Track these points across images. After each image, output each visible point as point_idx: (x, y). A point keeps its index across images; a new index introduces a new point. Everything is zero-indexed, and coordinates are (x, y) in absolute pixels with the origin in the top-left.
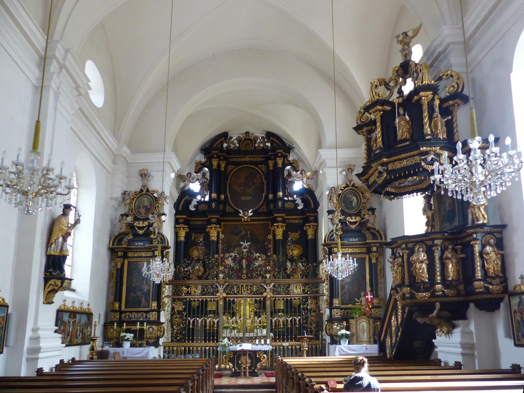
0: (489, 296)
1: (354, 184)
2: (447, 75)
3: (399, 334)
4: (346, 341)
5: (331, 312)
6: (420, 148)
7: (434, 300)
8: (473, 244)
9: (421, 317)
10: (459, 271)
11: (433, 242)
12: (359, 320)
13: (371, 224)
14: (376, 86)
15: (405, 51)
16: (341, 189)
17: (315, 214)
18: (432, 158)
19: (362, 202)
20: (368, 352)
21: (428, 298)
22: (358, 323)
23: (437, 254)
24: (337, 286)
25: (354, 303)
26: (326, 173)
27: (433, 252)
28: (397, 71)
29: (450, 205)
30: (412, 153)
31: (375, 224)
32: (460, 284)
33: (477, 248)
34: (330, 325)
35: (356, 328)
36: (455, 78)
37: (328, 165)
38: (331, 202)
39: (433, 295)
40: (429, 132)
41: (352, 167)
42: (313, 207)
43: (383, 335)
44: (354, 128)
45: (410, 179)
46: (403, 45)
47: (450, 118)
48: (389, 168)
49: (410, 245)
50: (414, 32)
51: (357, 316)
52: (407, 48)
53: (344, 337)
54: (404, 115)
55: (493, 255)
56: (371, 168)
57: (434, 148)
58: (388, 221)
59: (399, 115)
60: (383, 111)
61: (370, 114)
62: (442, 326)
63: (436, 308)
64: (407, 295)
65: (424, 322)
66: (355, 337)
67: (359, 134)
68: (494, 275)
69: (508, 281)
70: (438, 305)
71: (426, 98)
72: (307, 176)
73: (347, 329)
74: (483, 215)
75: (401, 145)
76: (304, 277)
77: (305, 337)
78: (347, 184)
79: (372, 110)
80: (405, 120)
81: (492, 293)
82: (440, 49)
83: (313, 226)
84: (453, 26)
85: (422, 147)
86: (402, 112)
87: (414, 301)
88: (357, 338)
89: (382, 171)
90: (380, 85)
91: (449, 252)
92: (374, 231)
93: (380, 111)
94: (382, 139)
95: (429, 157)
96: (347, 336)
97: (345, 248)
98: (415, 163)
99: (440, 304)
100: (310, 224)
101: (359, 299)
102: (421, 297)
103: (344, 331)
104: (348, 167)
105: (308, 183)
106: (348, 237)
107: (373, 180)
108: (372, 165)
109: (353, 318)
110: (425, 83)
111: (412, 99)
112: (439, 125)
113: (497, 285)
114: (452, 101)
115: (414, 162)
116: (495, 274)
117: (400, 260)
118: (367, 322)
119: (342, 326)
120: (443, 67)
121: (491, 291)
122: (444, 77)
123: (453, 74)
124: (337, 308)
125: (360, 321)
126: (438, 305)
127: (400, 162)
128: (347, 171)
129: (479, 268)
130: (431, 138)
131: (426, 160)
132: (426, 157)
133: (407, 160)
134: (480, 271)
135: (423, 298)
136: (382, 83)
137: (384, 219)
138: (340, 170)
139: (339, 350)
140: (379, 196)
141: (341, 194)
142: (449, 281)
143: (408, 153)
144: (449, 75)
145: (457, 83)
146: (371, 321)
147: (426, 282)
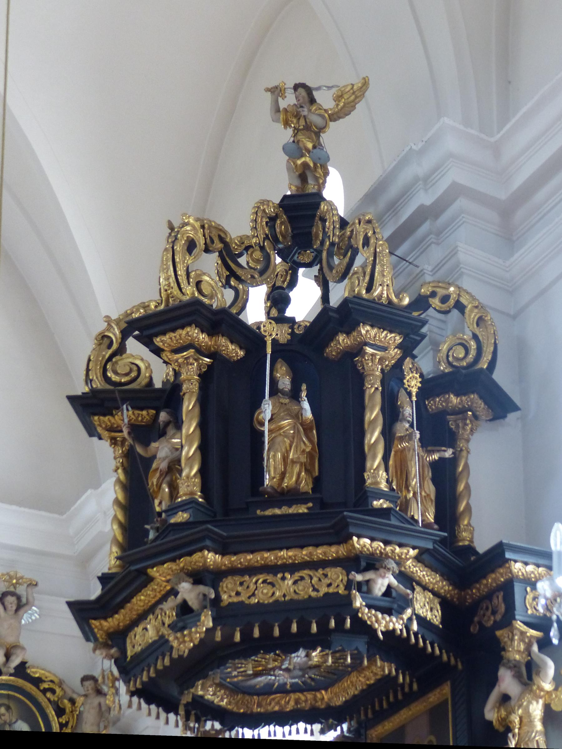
1: (23, 665)
6: (351, 538)
14: (191, 246)
15: (302, 156)
18: (389, 587)
28: (272, 220)
30: (319, 553)
36: (472, 316)
40: (383, 486)
41: (21, 590)
44: (72, 399)
45: (299, 657)
46: (297, 131)
47: (448, 453)
48: (225, 597)
50: (338, 98)
52: (310, 145)
54: (295, 395)
56: (144, 585)
57: (398, 550)
59: (274, 391)
60: (214, 355)
61: (157, 351)
67: (91, 431)
71: (379, 354)
75: (277, 511)
79: (166, 338)
80: (297, 416)
85: (359, 537)
86: (285, 383)
89: (194, 603)
90: (207, 250)
94: (202, 472)
98: (326, 594)
107: (151, 635)
108: (153, 572)
110: (380, 296)
111: (327, 345)
112: (414, 469)
114: (457, 395)
115: (324, 590)
120: (428, 268)
122: (435, 302)
123: (463, 300)
127: (270, 578)
130: (388, 510)
131: (369, 591)
132: (369, 575)
133: (297, 576)
136: (212, 241)
140: (163, 715)
143: (302, 547)
144: (452, 302)
145: (475, 337)
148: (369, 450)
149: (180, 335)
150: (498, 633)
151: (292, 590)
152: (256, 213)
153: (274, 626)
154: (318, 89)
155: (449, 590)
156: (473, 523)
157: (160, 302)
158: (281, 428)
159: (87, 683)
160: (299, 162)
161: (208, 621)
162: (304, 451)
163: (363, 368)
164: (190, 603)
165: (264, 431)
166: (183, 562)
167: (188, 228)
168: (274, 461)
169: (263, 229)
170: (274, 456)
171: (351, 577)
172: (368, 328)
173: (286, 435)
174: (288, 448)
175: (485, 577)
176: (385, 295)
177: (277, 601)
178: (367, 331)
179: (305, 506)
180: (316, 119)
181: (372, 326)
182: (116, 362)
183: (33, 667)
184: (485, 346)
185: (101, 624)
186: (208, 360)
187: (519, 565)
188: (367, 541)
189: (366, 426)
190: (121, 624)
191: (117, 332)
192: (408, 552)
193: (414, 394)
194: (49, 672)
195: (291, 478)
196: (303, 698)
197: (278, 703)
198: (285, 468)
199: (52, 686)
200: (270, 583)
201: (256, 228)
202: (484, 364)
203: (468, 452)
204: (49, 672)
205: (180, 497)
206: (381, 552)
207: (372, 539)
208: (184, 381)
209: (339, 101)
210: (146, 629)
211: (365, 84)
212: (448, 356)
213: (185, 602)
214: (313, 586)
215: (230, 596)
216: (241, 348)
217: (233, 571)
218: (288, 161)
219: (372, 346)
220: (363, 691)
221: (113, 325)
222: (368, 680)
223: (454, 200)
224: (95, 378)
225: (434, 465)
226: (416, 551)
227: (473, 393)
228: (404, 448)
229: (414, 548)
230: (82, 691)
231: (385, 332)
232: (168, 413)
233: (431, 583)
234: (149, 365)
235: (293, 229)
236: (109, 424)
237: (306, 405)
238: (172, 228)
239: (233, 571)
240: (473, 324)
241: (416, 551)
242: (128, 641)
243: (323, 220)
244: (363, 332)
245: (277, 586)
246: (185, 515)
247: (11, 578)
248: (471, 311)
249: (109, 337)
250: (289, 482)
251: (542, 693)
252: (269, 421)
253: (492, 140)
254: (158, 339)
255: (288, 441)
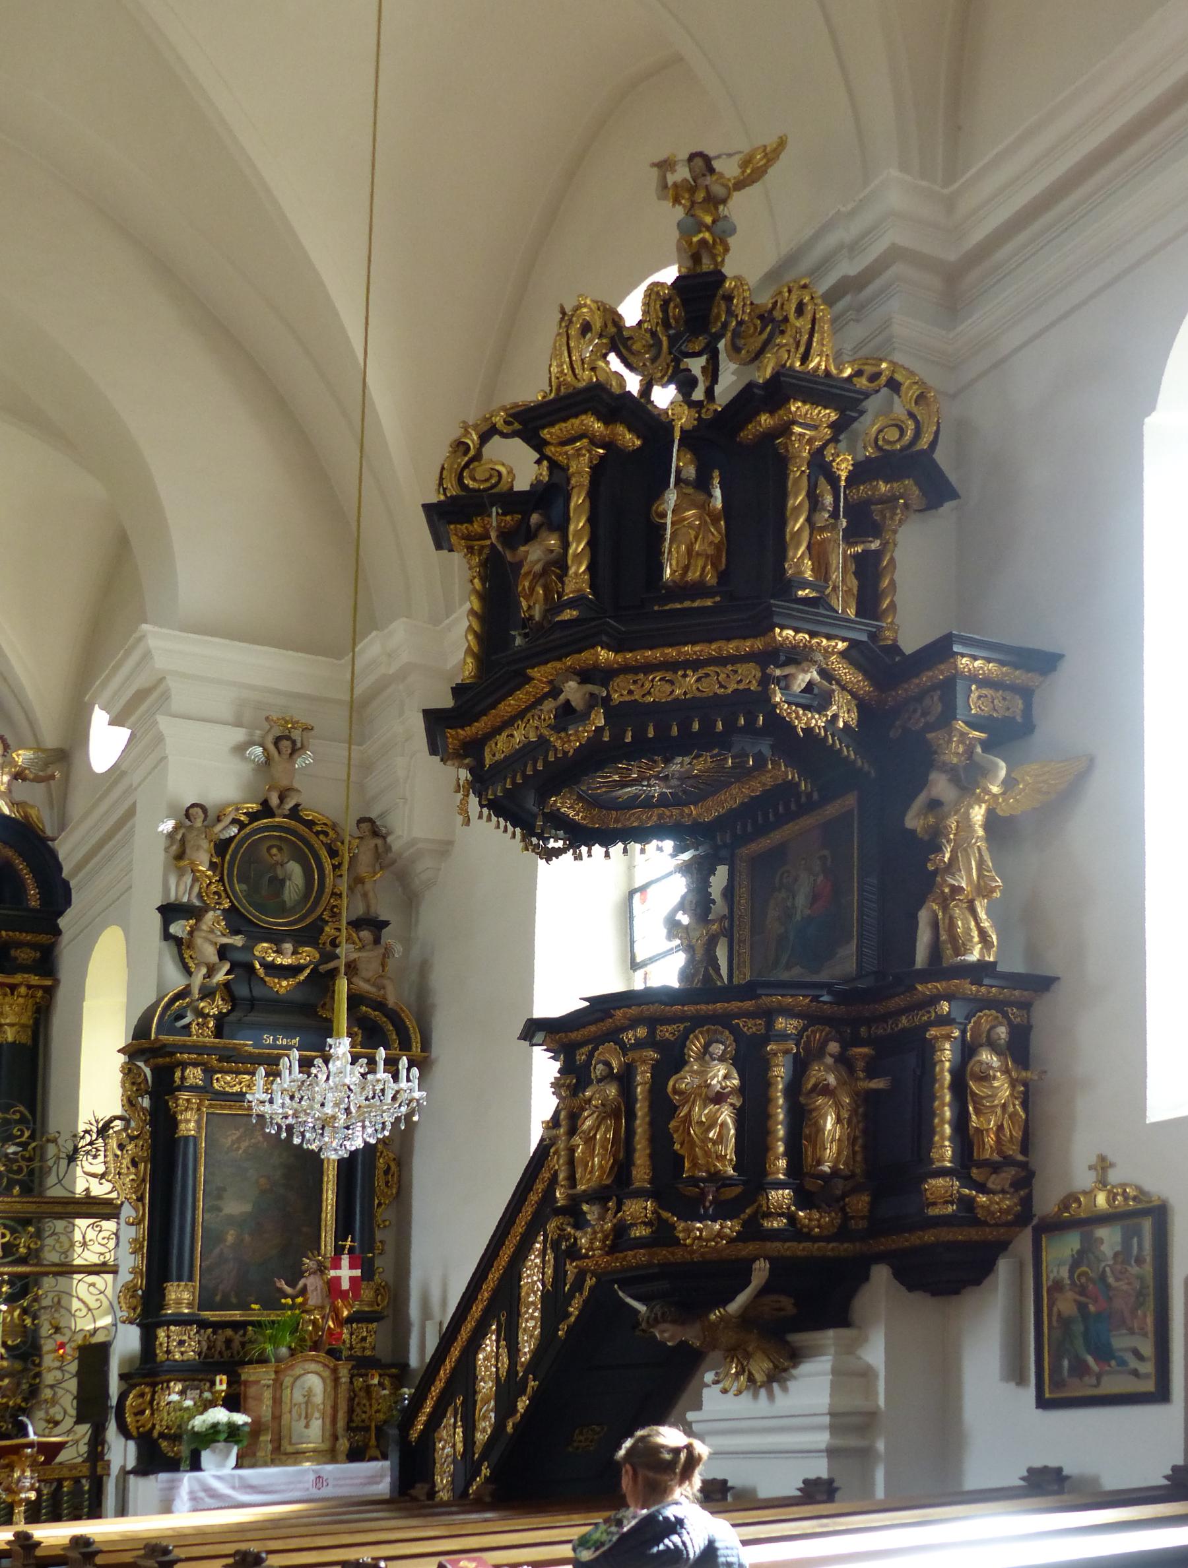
0: (973, 1234)
2: (874, 377)
3: (522, 1404)
4: (227, 1455)
5: (148, 1339)
6: (773, 630)
7: (751, 1248)
8: (936, 1038)
9: (674, 1322)
10: (855, 1139)
11: (770, 1025)
12: (291, 1367)
13: (367, 981)
14: (586, 328)
15: (700, 232)
16: (235, 821)
17: (43, 938)
19: (328, 890)
20: (327, 1492)
21: (731, 1241)
22: (288, 1381)
23: (780, 1072)
24: (188, 1229)
25: (272, 1302)
26: (168, 740)
27: (765, 1064)
29: (815, 898)
30: (731, 648)
31: (386, 982)
32: (855, 1190)
33: (947, 1055)
34: (142, 1395)
35: (277, 1401)
37: (178, 702)
38: (181, 873)
39: (752, 1231)
40: (808, 575)
41: (296, 735)
42: (34, 903)
43: (422, 1418)
47: (875, 545)
49: (666, 1032)
50: (745, 164)
51: (284, 1351)
53: (223, 1436)
55: (1002, 1088)
57: (825, 642)
58: (441, 980)
60: (609, 445)
62: (748, 1356)
63: (749, 1282)
64: (640, 1232)
65: (681, 1342)
66: (266, 1438)
68: (996, 1157)
69: (1037, 1183)
70: (761, 1271)
72: (13, 763)
73: (233, 1403)
74: (983, 934)
76: (17, 1190)
77: (31, 1445)
78: (265, 803)
79: (555, 430)
81: (985, 1223)
82: (848, 268)
83: (29, 987)
84: (924, 183)
85: (782, 628)
86: (690, 472)
87: (663, 1254)
88: (280, 1439)
91: (828, 1069)
92: (374, 1014)
93: (594, 442)
95: (801, 677)
96: (233, 1433)
97: (238, 1073)
98: (736, 690)
99: (771, 1270)
100: (18, 978)
101: (292, 1285)
102: (700, 1238)
103: (220, 1415)
104: (277, 732)
105: (18, 797)
106: (252, 1026)
108: (535, 673)
109: (262, 1360)
113: (1003, 1191)
114: (886, 483)
115: (732, 687)
116: (1000, 1152)
117: (612, 1091)
118: (327, 1373)
119: (207, 1395)
121: (980, 1214)
123: (898, 377)
124: (181, 1321)
125: (298, 1371)
126: (761, 1271)
128: (271, 748)
129: (947, 1129)
132: (787, 671)
133: (701, 673)
134: (951, 1139)
135: (708, 1240)
137: (424, 969)
138: (239, 735)
139: (191, 1492)
141: (232, 839)
142: (822, 1176)
143: (710, 641)
144: (883, 379)
146: (344, 1373)
147: (730, 1178)
148: (792, 538)
149: (572, 425)
150: (930, 736)
151: (694, 688)
152: (650, 295)
153: (671, 725)
154: (719, 157)
155: (870, 692)
156: (897, 621)
157: (548, 392)
158: (684, 519)
159: (363, 825)
160: (695, 239)
161: (600, 719)
162: (711, 543)
163: (787, 451)
164: (573, 704)
165: (666, 524)
166: (569, 661)
167: (585, 310)
168: (678, 553)
169: (657, 313)
170: (678, 547)
171: (768, 671)
172: (799, 404)
173: (690, 526)
174: (693, 540)
175: (917, 675)
176: (823, 367)
177: (677, 700)
178: (798, 408)
179: (712, 600)
180: (718, 190)
181: (804, 402)
182: (474, 469)
183: (306, 810)
184: (926, 425)
185: (457, 733)
186: (601, 451)
187: (965, 660)
188: (791, 633)
189: (788, 513)
190: (480, 733)
191: (475, 437)
192: (837, 644)
193: (843, 478)
194: (323, 816)
195: (694, 573)
196: (668, 813)
197: (638, 818)
198: (689, 561)
199: (325, 828)
200: (668, 681)
201: (648, 312)
202: (924, 444)
203: (895, 545)
204: (323, 816)
205: (567, 594)
206: (805, 644)
207: (797, 631)
208: (573, 474)
209: (747, 167)
210: (512, 736)
211: (782, 144)
212: (876, 440)
213: (568, 702)
214: (719, 683)
215: (622, 695)
216: (638, 438)
217: (626, 669)
218: (678, 241)
219: (801, 425)
220: (743, 804)
221: (470, 430)
222: (753, 791)
223: (887, 267)
224: (449, 486)
225: (856, 557)
226: (846, 644)
227: (908, 477)
228: (824, 540)
229: (844, 640)
230: (357, 833)
231: (820, 408)
232: (540, 514)
233: (852, 682)
234: (512, 469)
235: (686, 313)
236: (465, 531)
237: (718, 493)
238: (564, 313)
239: (626, 669)
240: (910, 403)
241: (846, 644)
242: (487, 750)
243: (729, 298)
244: (793, 409)
245: (677, 685)
246: (575, 613)
247: (287, 722)
248: (909, 388)
249: (467, 444)
250: (693, 575)
251: (987, 797)
252: (673, 511)
253: (946, 191)
254: (546, 431)
255: (693, 533)
